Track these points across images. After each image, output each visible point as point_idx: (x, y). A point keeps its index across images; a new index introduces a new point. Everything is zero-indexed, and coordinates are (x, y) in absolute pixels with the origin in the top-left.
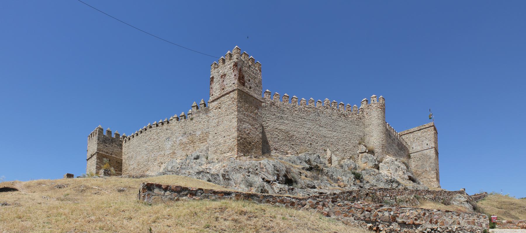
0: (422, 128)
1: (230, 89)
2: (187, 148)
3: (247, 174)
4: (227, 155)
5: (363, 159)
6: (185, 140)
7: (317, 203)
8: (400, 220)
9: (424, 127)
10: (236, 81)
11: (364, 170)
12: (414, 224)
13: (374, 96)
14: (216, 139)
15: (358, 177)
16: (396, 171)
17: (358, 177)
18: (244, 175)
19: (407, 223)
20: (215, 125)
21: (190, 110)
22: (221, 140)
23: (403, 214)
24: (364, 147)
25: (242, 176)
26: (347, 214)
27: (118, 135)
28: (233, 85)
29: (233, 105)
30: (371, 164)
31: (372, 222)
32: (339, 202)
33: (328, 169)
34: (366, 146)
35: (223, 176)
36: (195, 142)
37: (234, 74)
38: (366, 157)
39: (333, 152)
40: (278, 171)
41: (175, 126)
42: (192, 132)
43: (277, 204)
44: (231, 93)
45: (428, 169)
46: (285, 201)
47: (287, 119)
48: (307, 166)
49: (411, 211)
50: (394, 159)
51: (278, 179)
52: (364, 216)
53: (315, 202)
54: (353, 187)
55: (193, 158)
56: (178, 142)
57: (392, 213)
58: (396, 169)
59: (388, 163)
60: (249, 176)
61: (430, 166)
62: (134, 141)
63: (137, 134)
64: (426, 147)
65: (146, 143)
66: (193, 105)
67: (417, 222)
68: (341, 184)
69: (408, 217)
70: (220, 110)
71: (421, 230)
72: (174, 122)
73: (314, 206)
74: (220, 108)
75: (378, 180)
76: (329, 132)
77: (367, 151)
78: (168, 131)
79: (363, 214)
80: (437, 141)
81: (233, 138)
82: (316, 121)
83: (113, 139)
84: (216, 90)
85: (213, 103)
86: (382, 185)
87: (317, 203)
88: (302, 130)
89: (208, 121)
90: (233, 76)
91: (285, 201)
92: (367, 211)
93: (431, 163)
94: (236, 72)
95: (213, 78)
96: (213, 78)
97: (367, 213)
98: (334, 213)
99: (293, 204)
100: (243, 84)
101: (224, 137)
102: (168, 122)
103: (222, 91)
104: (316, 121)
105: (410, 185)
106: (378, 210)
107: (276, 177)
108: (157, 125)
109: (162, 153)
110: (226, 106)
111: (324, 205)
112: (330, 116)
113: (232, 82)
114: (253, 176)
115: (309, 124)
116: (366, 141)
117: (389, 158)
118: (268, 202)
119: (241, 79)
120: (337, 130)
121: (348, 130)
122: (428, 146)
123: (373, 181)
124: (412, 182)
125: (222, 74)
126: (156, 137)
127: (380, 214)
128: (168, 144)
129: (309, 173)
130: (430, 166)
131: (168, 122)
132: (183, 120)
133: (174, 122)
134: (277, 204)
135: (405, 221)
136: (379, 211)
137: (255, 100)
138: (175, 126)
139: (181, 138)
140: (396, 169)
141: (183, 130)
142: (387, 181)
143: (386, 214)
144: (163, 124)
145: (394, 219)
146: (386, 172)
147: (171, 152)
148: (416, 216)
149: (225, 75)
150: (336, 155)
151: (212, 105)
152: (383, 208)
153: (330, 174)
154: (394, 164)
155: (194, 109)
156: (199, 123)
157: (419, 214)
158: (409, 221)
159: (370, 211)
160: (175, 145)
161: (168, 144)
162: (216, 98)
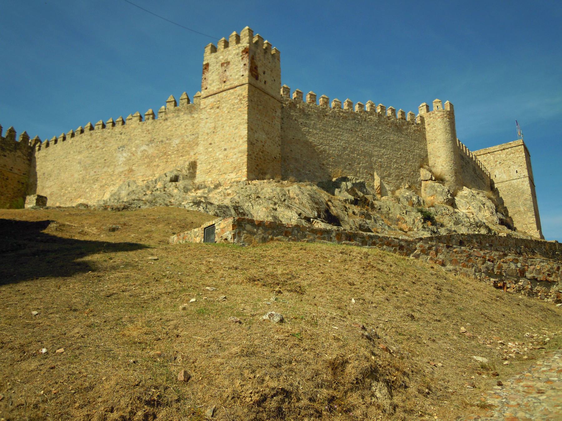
0: (508, 146)
1: (236, 83)
2: (155, 164)
3: (271, 206)
4: (229, 177)
5: (427, 190)
6: (151, 151)
7: (430, 248)
8: (528, 275)
9: (509, 146)
10: (247, 73)
11: (433, 206)
12: (547, 280)
13: (437, 100)
14: (211, 152)
15: (428, 218)
16: (480, 210)
17: (428, 218)
18: (267, 208)
19: (538, 280)
20: (209, 131)
21: (163, 107)
22: (220, 155)
23: (532, 267)
24: (428, 172)
25: (264, 209)
26: (466, 263)
27: (26, 137)
28: (241, 78)
29: (242, 106)
30: (441, 199)
31: (495, 276)
32: (455, 248)
33: (381, 204)
34: (431, 171)
35: (235, 210)
36: (169, 155)
37: (242, 63)
38: (432, 187)
39: (382, 178)
40: (316, 203)
41: (135, 128)
42: (165, 139)
43: (385, 247)
44: (238, 88)
45: (522, 209)
46: (393, 244)
47: (314, 127)
48: (351, 197)
49: (542, 264)
50: (474, 192)
51: (319, 216)
52: (487, 268)
53: (427, 246)
54: (423, 232)
55: (168, 179)
56: (139, 153)
57: (519, 265)
58: (480, 207)
59: (466, 197)
60: (276, 210)
61: (525, 205)
62: (57, 149)
63: (64, 139)
64: (515, 175)
65: (80, 152)
66: (169, 99)
67: (551, 279)
68: (404, 226)
69: (539, 272)
70: (218, 110)
71: (557, 288)
72: (133, 123)
73: (425, 252)
74: (218, 108)
75: (457, 223)
76: (376, 149)
77: (434, 178)
78: (123, 137)
79: (485, 265)
80: (531, 166)
81: (240, 152)
82: (357, 131)
83: (17, 144)
84: (212, 81)
85: (205, 100)
86: (463, 230)
87: (430, 248)
88: (334, 144)
89: (193, 125)
90: (242, 65)
91: (393, 244)
92: (489, 260)
93: (526, 200)
94: (246, 61)
95: (207, 65)
96: (207, 65)
97: (489, 263)
98: (451, 261)
99: (401, 248)
100: (257, 78)
101: (225, 150)
102: (124, 123)
103: (223, 84)
104: (357, 131)
105: (504, 232)
106: (502, 260)
107: (316, 214)
108: (104, 126)
109: (110, 170)
110: (228, 106)
111: (437, 252)
112: (376, 125)
113: (239, 72)
114: (282, 209)
115: (346, 136)
116: (431, 163)
117: (466, 191)
118: (374, 244)
119: (254, 71)
120: (387, 145)
121: (402, 146)
122: (518, 174)
123: (450, 225)
124: (506, 228)
125: (223, 61)
126: (101, 145)
127: (505, 266)
128: (122, 157)
129: (357, 209)
130: (525, 205)
131: (124, 123)
132: (151, 121)
133: (133, 123)
134: (385, 247)
135: (536, 276)
136: (503, 262)
137: (272, 99)
138: (135, 128)
139: (144, 147)
140: (480, 207)
141: (150, 136)
142: (471, 224)
143: (513, 266)
144: (114, 124)
145: (522, 273)
146: (464, 211)
147: (127, 168)
148: (548, 271)
149: (228, 63)
150: (388, 183)
151: (204, 103)
152: (508, 257)
153: (385, 210)
154: (477, 200)
155: (171, 106)
156: (176, 125)
157: (552, 268)
158: (541, 277)
159: (492, 262)
160: (133, 158)
161: (122, 157)
162: (211, 93)
